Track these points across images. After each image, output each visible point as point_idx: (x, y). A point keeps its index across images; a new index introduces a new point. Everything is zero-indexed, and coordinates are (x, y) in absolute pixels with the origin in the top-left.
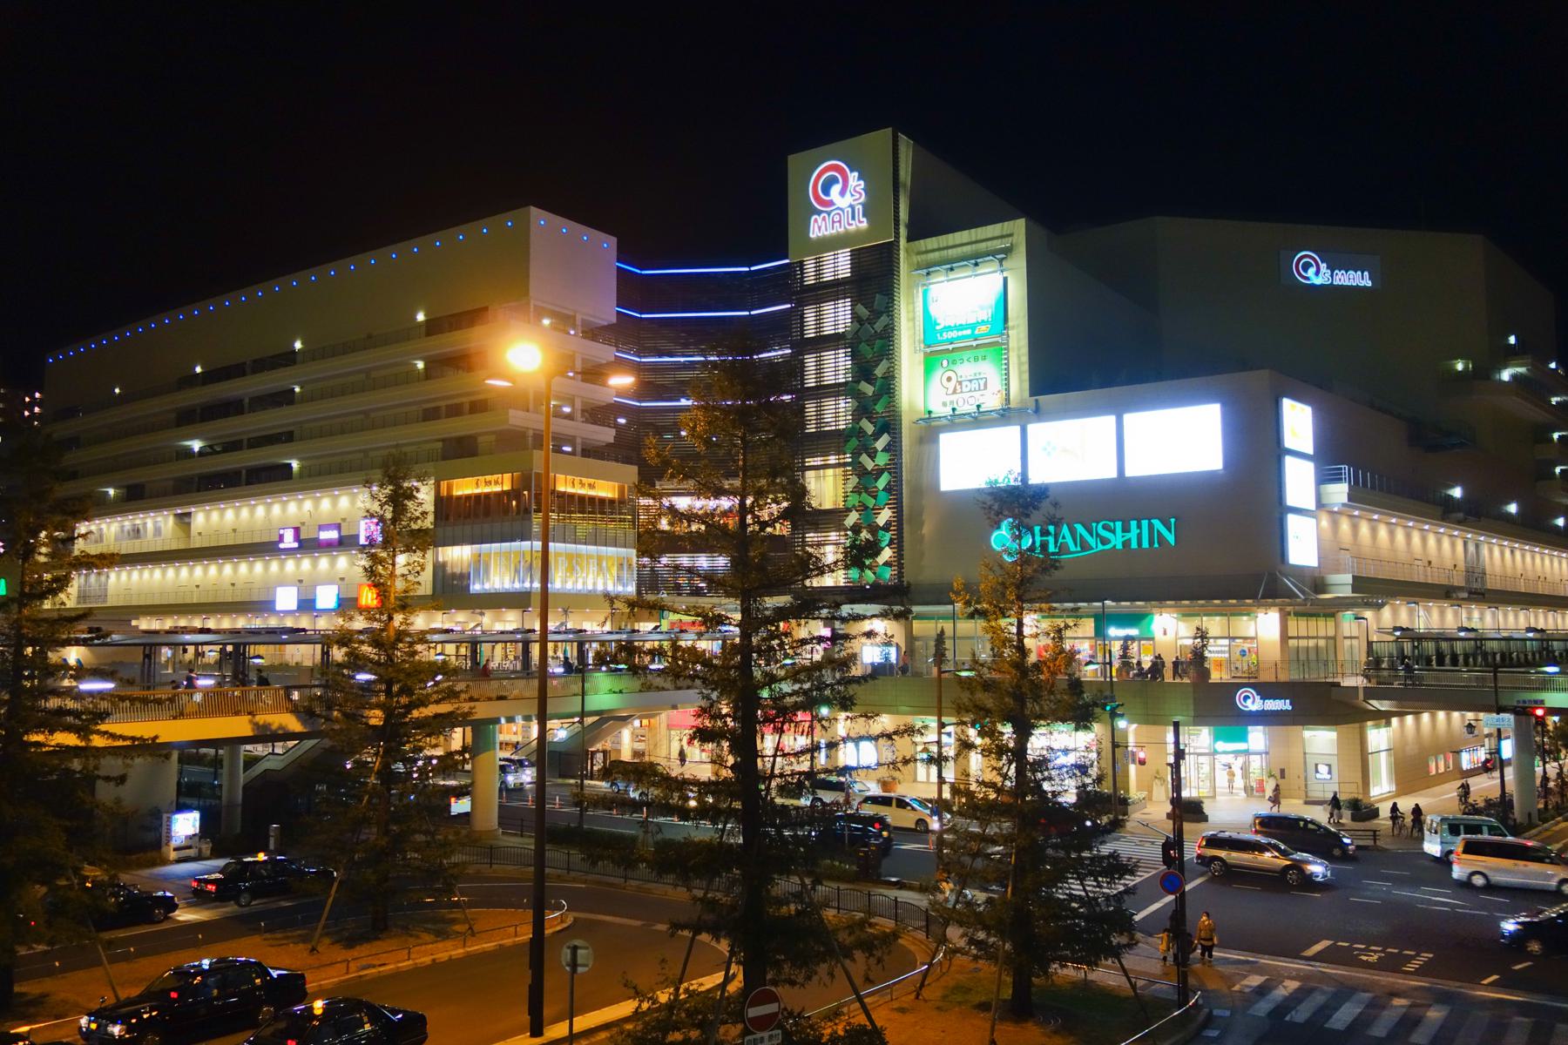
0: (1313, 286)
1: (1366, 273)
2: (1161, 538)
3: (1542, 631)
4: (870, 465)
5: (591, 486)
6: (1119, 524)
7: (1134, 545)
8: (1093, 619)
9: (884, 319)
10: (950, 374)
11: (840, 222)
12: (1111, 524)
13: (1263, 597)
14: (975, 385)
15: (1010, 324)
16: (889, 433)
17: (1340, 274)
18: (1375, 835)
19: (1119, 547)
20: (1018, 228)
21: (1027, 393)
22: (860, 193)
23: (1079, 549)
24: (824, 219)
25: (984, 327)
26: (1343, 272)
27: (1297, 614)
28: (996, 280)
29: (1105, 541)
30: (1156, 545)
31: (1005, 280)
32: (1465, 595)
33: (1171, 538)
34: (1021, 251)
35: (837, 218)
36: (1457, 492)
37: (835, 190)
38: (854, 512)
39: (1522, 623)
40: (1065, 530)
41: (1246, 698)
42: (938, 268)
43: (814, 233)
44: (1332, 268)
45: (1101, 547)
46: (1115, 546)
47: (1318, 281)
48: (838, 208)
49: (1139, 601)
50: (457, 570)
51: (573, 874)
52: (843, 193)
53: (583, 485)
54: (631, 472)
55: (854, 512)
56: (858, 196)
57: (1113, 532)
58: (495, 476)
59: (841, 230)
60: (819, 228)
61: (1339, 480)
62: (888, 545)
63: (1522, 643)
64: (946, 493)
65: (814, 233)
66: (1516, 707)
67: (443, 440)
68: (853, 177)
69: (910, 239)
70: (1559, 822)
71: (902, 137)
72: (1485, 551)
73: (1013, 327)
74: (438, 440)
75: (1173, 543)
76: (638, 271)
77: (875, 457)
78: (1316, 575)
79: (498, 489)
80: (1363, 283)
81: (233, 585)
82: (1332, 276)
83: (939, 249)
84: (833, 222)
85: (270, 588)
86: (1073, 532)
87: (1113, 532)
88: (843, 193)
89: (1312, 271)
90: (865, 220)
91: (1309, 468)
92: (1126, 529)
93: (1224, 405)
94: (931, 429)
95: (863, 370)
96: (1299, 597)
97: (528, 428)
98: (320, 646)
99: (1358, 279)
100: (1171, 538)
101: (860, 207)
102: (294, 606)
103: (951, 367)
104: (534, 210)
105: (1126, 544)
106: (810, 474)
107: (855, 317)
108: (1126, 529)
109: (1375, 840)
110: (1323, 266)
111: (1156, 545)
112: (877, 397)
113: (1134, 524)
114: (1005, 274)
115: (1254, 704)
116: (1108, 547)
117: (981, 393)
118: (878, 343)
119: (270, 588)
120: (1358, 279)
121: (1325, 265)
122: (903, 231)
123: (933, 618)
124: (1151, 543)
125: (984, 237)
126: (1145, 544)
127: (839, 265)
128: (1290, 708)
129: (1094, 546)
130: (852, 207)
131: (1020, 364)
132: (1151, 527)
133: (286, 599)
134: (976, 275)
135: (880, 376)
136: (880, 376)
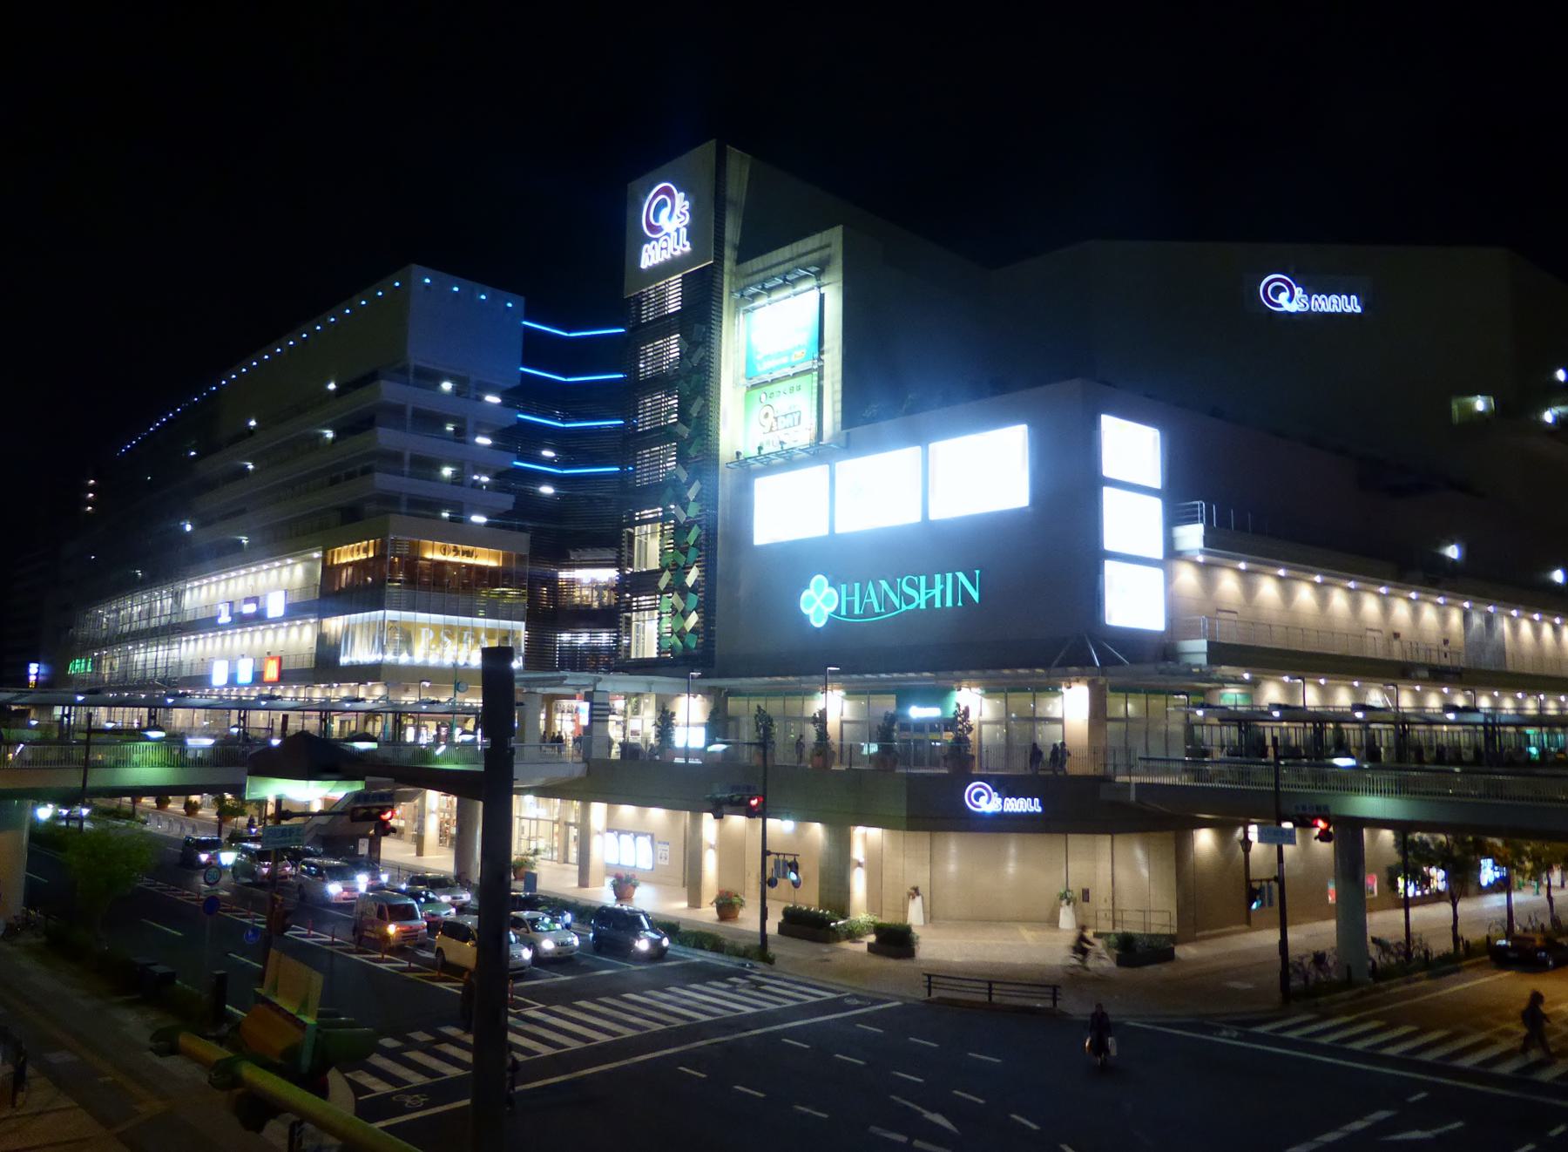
0: (1289, 314)
2: (966, 596)
5: (468, 554)
6: (923, 579)
7: (938, 604)
8: (894, 696)
9: (701, 352)
10: (768, 409)
12: (916, 579)
14: (788, 421)
17: (1320, 299)
18: (1055, 994)
19: (923, 606)
20: (834, 238)
22: (684, 215)
23: (883, 610)
25: (799, 353)
26: (1324, 296)
27: (1116, 689)
28: (814, 296)
29: (909, 600)
31: (822, 297)
32: (1425, 674)
33: (975, 595)
34: (838, 263)
36: (1453, 552)
37: (665, 212)
43: (645, 263)
44: (1308, 293)
45: (904, 608)
46: (919, 605)
47: (1293, 307)
53: (456, 551)
56: (682, 218)
57: (917, 589)
59: (668, 257)
60: (650, 257)
61: (1193, 520)
62: (695, 610)
65: (645, 263)
68: (680, 197)
69: (740, 261)
70: (1417, 980)
72: (1505, 626)
75: (870, 583)
76: (566, 334)
78: (1167, 641)
80: (1349, 309)
81: (202, 660)
84: (662, 249)
85: (207, 663)
87: (917, 589)
90: (688, 244)
92: (930, 585)
93: (1031, 426)
94: (748, 470)
96: (1094, 664)
97: (401, 493)
99: (1345, 304)
100: (975, 595)
103: (770, 401)
104: (415, 267)
105: (930, 602)
109: (1055, 1000)
110: (1298, 291)
111: (960, 604)
113: (938, 577)
115: (988, 803)
116: (912, 607)
117: (794, 428)
118: (695, 377)
119: (207, 663)
120: (1345, 304)
121: (682, 194)
122: (729, 254)
123: (744, 695)
124: (955, 600)
126: (949, 603)
128: (1039, 810)
129: (898, 607)
130: (678, 230)
131: (834, 392)
132: (955, 579)
134: (795, 295)
135: (695, 415)
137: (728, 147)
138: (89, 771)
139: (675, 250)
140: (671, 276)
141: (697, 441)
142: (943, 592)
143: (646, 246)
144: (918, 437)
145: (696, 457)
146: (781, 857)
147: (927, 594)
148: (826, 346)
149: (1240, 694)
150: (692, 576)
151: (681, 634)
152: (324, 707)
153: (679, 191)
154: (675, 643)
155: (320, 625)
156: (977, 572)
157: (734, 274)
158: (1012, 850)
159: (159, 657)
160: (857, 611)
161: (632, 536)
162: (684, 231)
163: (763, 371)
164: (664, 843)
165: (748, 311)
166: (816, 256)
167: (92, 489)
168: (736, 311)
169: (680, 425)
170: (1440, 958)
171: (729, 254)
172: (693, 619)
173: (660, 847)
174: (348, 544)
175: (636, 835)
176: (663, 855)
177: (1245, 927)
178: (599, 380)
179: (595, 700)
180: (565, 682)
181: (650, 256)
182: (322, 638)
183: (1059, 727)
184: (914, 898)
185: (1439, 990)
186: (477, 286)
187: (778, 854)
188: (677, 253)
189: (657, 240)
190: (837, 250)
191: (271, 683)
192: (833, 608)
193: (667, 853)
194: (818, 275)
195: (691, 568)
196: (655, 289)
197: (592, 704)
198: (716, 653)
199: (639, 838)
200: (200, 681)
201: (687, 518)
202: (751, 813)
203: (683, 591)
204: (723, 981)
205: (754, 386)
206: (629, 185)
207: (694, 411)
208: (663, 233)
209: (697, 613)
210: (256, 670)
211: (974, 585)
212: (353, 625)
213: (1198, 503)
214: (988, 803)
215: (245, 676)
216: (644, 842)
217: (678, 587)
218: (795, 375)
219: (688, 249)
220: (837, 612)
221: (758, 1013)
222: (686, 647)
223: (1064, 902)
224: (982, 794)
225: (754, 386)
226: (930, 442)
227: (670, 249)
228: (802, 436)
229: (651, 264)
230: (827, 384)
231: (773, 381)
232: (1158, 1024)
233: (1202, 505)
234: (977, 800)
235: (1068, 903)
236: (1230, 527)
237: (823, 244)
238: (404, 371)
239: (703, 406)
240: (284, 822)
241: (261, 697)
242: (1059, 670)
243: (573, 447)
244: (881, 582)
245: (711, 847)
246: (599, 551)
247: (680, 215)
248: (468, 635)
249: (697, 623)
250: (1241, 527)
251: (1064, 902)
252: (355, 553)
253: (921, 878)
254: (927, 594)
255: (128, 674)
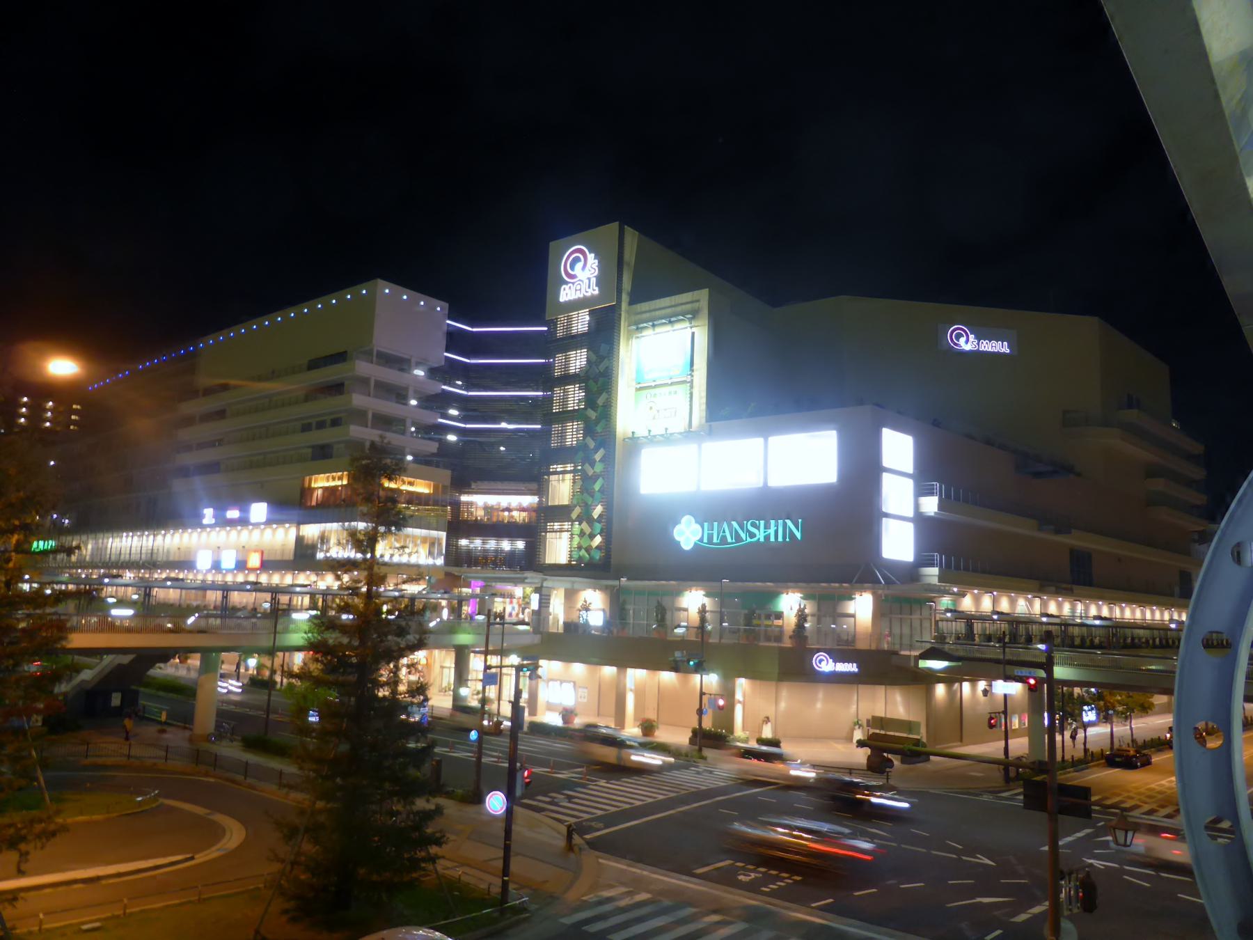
1: (1005, 343)
2: (792, 535)
3: (1110, 619)
4: (590, 472)
5: (411, 484)
6: (762, 523)
7: (772, 539)
11: (580, 290)
12: (757, 522)
13: (856, 582)
15: (695, 367)
16: (604, 448)
17: (985, 342)
19: (762, 540)
20: (703, 296)
21: (704, 420)
23: (734, 541)
24: (570, 287)
29: (752, 535)
30: (788, 540)
33: (798, 535)
34: (705, 311)
35: (578, 287)
37: (579, 266)
38: (578, 507)
39: (1093, 611)
40: (725, 526)
41: (821, 661)
42: (645, 325)
44: (979, 338)
46: (759, 539)
47: (968, 347)
48: (580, 280)
49: (846, 583)
50: (310, 542)
51: (249, 780)
52: (584, 267)
53: (334, 479)
54: (445, 475)
55: (578, 507)
56: (593, 271)
57: (758, 528)
58: (340, 474)
59: (582, 296)
61: (932, 494)
62: (599, 534)
63: (200, 593)
64: (882, 520)
66: (1016, 676)
67: (313, 447)
68: (591, 257)
69: (631, 303)
70: (1069, 772)
71: (628, 230)
73: (697, 370)
74: (308, 447)
77: (594, 466)
79: (339, 483)
80: (1003, 350)
81: (179, 549)
82: (978, 344)
83: (650, 311)
84: (576, 290)
86: (730, 526)
87: (758, 528)
88: (584, 267)
89: (962, 340)
90: (597, 289)
91: (909, 484)
92: (767, 527)
95: (590, 401)
96: (881, 583)
98: (221, 592)
100: (798, 535)
101: (595, 279)
102: (233, 566)
104: (380, 282)
105: (767, 538)
106: (553, 478)
107: (588, 361)
108: (767, 527)
110: (972, 337)
111: (788, 540)
112: (597, 421)
113: (773, 522)
114: (694, 330)
115: (826, 665)
116: (755, 539)
121: (593, 255)
122: (625, 298)
124: (784, 537)
125: (680, 302)
126: (780, 539)
127: (581, 322)
129: (744, 539)
130: (589, 279)
131: (701, 398)
132: (785, 525)
133: (203, 562)
134: (674, 330)
135: (601, 404)
136: (601, 404)
137: (626, 227)
138: (277, 635)
139: (586, 292)
140: (580, 310)
141: (602, 423)
142: (776, 532)
143: (564, 286)
144: (765, 432)
145: (601, 432)
146: (712, 696)
147: (765, 532)
148: (695, 367)
149: (951, 600)
150: (598, 511)
151: (588, 549)
152: (325, 592)
153: (590, 253)
154: (584, 556)
155: (298, 530)
156: (800, 520)
157: (628, 312)
158: (821, 695)
159: (134, 545)
160: (715, 540)
161: (548, 481)
162: (594, 280)
163: (648, 380)
164: (584, 688)
165: (638, 337)
166: (688, 307)
167: (25, 405)
168: (628, 338)
169: (589, 410)
170: (1077, 761)
171: (625, 298)
172: (598, 540)
173: (580, 690)
174: (325, 473)
175: (562, 682)
176: (583, 696)
177: (959, 743)
178: (456, 355)
179: (543, 593)
180: (526, 581)
181: (567, 294)
182: (299, 540)
183: (853, 619)
184: (767, 723)
185: (1084, 777)
186: (418, 295)
187: (710, 694)
188: (588, 294)
189: (573, 283)
190: (704, 304)
191: (253, 570)
192: (699, 536)
193: (586, 694)
194: (693, 318)
195: (597, 506)
196: (568, 316)
197: (541, 595)
198: (612, 563)
199: (564, 684)
200: (186, 564)
201: (594, 472)
202: (675, 668)
203: (590, 521)
204: (545, 795)
205: (641, 388)
206: (552, 244)
207: (600, 401)
208: (577, 279)
209: (601, 536)
210: (240, 559)
211: (797, 528)
212: (329, 531)
213: (935, 483)
214: (826, 665)
215: (228, 561)
216: (568, 687)
217: (586, 517)
218: (672, 384)
219: (597, 292)
220: (701, 540)
221: (677, 796)
222: (591, 558)
223: (857, 727)
224: (823, 660)
225: (641, 388)
226: (769, 436)
227: (583, 291)
228: (679, 425)
229: (567, 300)
230: (695, 391)
231: (656, 386)
232: (957, 793)
233: (936, 485)
234: (820, 663)
235: (859, 728)
236: (951, 498)
237: (694, 299)
238: (370, 353)
239: (607, 399)
240: (488, 671)
241: (167, 579)
242: (858, 585)
243: (472, 409)
244: (733, 522)
245: (631, 690)
246: (492, 483)
247: (591, 269)
248: (410, 541)
249: (601, 542)
250: (957, 499)
251: (857, 727)
252: (331, 479)
253: (770, 711)
254: (765, 532)
255: (103, 557)
